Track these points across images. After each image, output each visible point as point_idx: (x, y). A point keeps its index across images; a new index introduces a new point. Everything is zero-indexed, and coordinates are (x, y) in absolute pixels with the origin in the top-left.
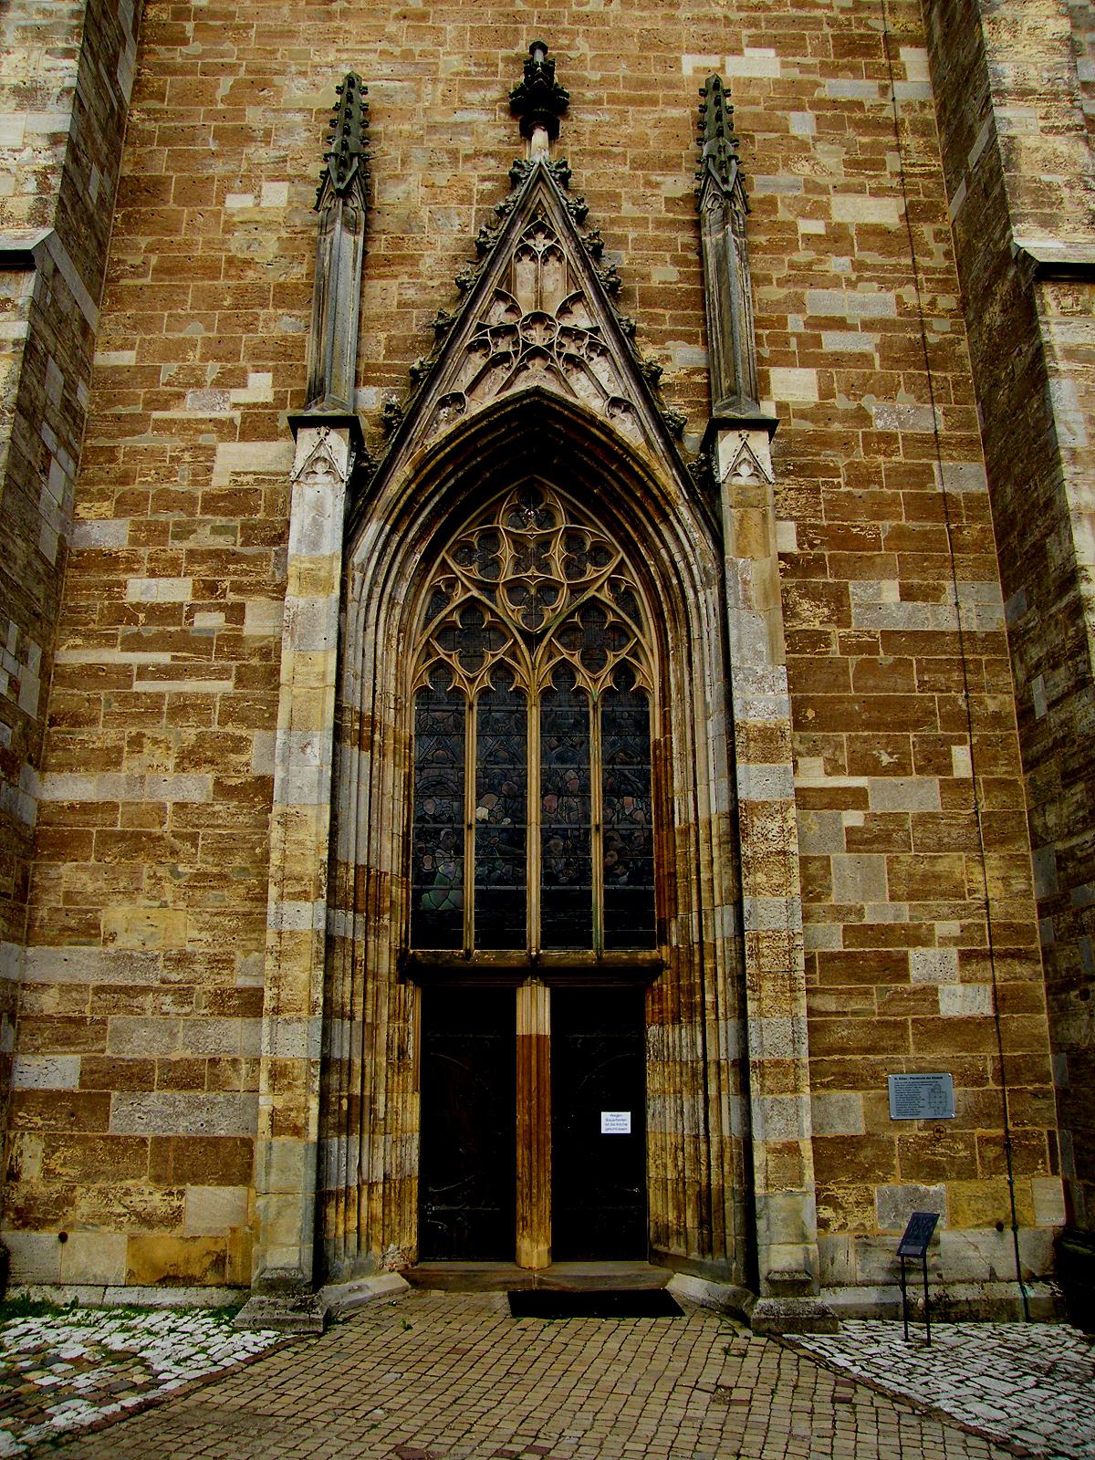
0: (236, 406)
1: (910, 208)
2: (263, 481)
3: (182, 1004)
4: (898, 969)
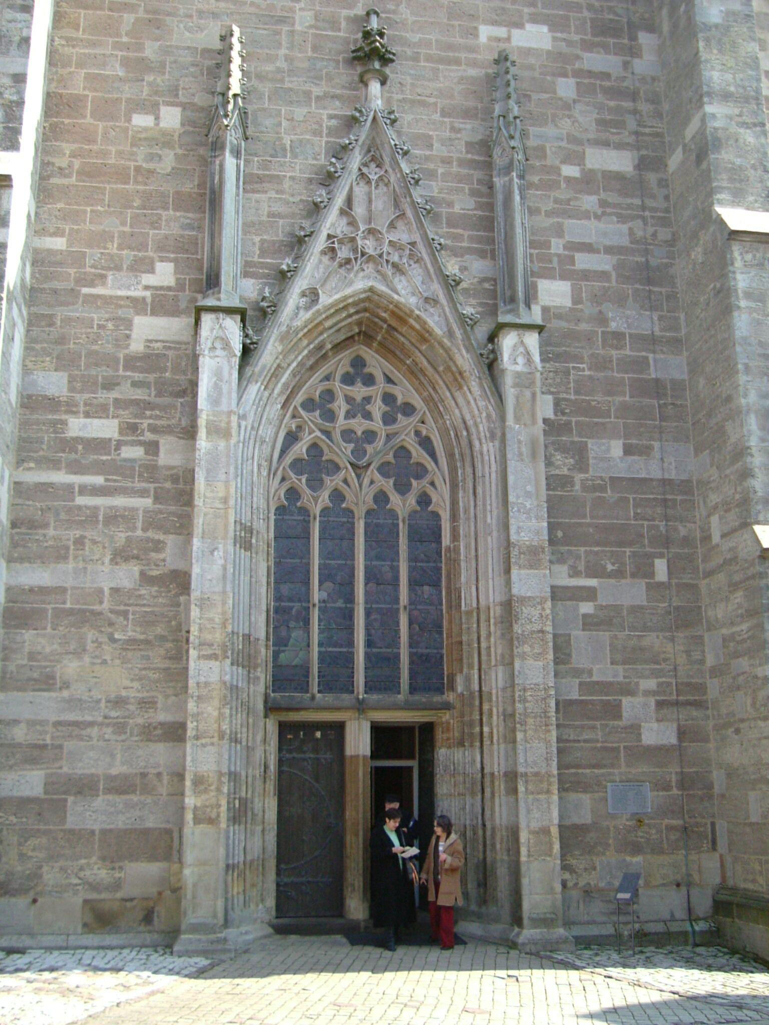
0: (147, 288)
1: (642, 159)
2: (170, 348)
3: (120, 734)
4: (614, 711)
